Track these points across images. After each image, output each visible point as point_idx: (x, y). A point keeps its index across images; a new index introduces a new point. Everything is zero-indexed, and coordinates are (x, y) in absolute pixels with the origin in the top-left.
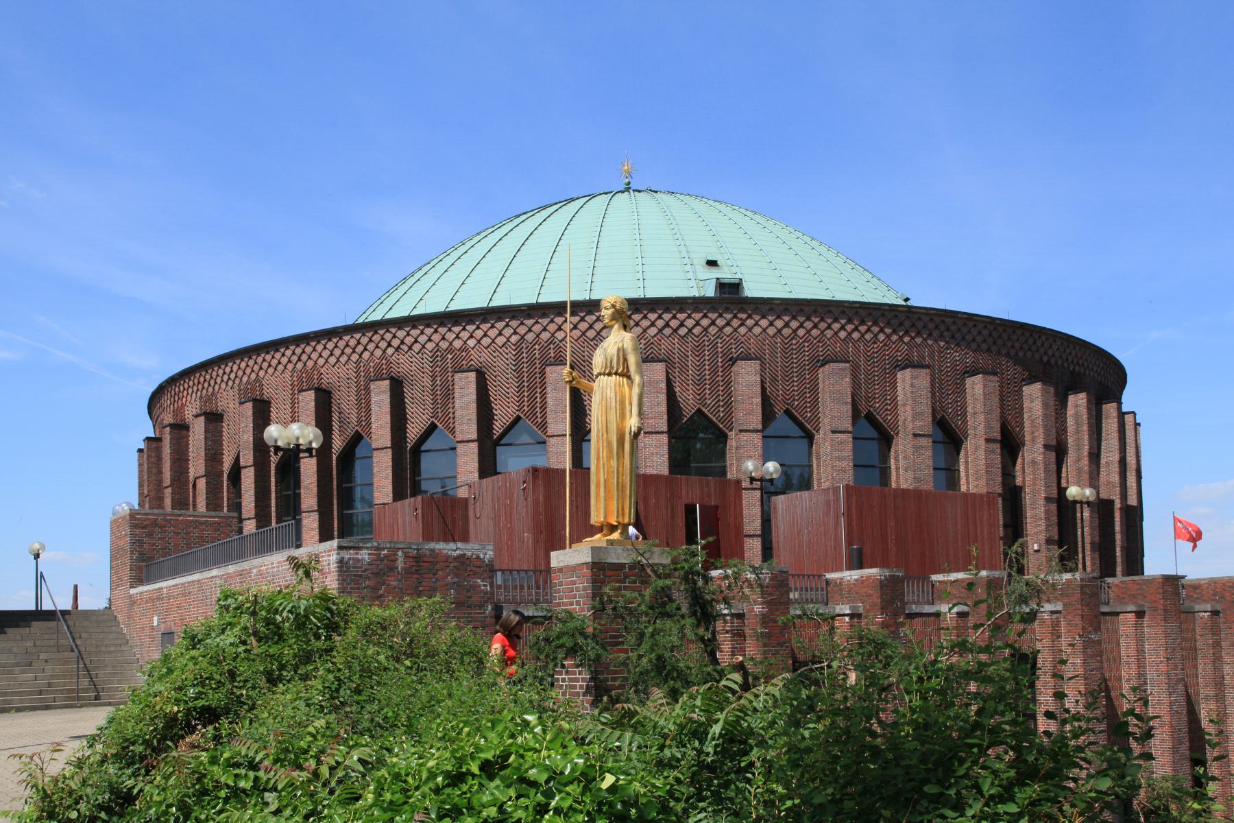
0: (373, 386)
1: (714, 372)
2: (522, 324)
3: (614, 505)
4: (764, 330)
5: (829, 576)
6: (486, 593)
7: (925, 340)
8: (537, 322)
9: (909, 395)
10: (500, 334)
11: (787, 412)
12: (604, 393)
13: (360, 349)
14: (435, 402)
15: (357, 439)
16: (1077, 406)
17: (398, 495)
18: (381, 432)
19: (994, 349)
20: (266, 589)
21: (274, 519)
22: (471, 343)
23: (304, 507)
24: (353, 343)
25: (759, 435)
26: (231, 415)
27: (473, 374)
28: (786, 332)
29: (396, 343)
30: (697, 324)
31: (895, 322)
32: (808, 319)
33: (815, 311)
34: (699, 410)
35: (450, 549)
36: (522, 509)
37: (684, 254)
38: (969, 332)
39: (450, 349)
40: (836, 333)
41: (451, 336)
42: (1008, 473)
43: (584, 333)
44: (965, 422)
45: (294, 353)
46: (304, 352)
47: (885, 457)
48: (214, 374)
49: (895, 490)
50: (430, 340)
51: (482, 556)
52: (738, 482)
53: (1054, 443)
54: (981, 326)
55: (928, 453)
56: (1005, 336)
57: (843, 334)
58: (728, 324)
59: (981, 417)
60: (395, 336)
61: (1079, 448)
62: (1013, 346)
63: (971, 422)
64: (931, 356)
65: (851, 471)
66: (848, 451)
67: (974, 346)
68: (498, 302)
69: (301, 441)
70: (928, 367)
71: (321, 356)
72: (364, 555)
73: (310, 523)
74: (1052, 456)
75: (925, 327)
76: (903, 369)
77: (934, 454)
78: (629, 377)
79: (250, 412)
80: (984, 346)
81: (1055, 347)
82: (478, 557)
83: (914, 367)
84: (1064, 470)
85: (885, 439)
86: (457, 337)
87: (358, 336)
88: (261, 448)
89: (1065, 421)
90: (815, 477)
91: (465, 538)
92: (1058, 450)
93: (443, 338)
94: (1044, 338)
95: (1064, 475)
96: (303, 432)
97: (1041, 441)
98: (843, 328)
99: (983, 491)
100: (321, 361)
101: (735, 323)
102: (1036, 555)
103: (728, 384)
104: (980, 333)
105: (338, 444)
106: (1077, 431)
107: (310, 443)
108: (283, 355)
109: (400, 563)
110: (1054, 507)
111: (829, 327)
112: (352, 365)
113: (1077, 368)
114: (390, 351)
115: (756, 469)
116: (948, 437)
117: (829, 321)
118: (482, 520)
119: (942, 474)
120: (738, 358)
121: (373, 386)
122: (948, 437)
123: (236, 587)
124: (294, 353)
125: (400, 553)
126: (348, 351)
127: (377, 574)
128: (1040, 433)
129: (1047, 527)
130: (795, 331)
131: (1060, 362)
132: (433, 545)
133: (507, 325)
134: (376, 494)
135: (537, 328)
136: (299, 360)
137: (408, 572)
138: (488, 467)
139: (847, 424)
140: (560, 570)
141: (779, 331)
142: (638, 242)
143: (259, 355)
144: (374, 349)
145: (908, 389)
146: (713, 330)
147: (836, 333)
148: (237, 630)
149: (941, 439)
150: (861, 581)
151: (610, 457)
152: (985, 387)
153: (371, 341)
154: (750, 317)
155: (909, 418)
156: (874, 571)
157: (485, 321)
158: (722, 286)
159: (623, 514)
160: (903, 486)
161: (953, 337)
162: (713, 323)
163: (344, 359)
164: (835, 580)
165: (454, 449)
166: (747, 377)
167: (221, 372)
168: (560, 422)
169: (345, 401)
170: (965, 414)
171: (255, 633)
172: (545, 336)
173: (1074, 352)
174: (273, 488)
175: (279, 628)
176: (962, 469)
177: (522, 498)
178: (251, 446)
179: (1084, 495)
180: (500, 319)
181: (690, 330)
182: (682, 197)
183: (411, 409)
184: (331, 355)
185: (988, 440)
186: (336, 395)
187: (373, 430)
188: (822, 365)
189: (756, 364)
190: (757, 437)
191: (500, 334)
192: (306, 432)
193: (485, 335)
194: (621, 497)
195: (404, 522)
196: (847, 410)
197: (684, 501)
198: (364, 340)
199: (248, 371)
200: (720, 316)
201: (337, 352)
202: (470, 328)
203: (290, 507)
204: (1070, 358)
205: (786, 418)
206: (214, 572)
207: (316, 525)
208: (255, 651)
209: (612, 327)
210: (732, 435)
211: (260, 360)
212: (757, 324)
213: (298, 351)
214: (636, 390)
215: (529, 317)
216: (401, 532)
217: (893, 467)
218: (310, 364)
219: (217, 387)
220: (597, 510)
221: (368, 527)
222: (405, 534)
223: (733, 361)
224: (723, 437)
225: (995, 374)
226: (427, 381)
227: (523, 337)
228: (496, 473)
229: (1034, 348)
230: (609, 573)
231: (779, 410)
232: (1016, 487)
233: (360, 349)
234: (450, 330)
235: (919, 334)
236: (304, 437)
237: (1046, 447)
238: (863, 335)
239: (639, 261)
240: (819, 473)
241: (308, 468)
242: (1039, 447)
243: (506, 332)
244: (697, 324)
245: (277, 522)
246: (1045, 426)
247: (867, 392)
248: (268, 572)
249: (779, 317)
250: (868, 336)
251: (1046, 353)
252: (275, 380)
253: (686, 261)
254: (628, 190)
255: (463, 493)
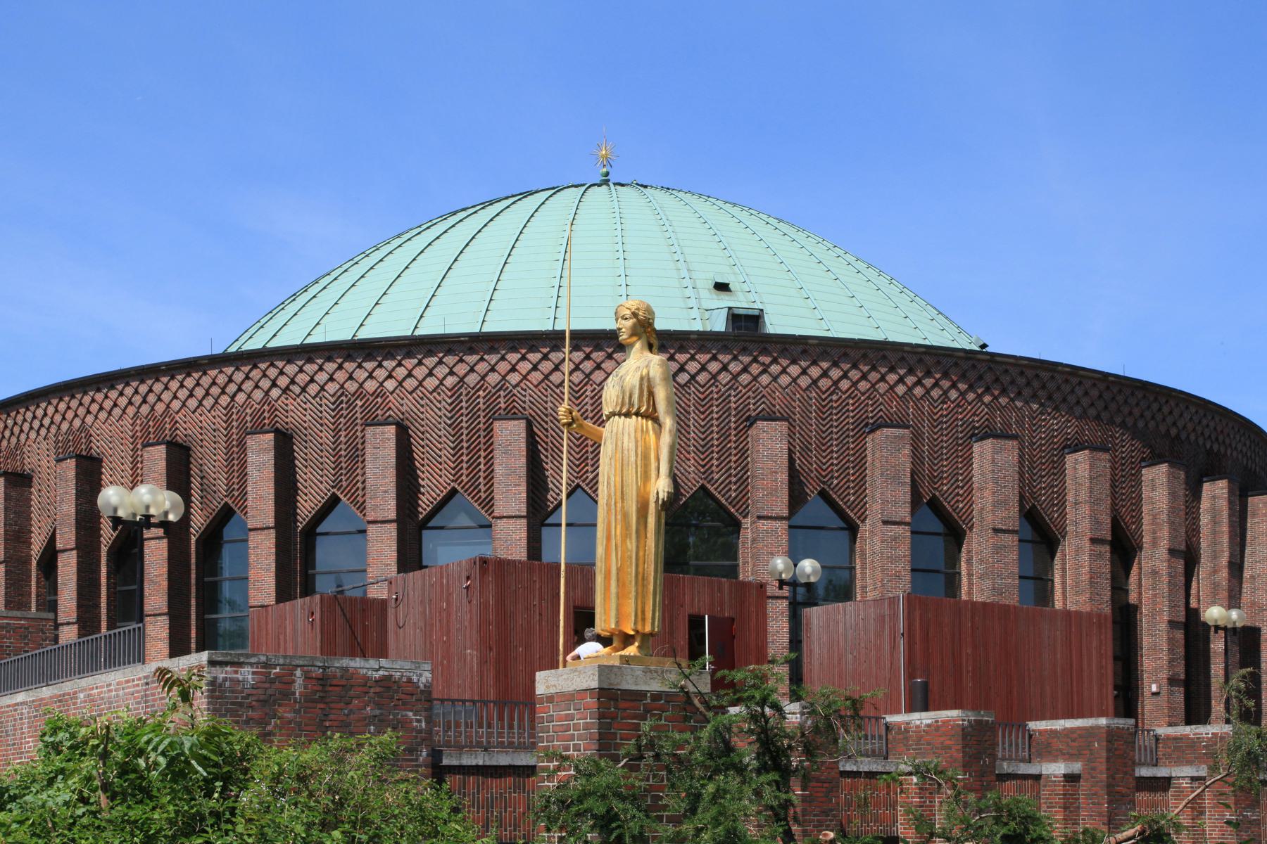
0: (251, 442)
1: (725, 436)
2: (461, 360)
3: (630, 607)
4: (794, 380)
5: (890, 719)
6: (420, 731)
7: (1012, 400)
8: (482, 359)
9: (989, 476)
10: (430, 374)
11: (823, 494)
12: (620, 439)
13: (232, 388)
14: (337, 465)
15: (225, 515)
16: (1214, 497)
17: (284, 593)
18: (260, 504)
19: (1104, 415)
20: (124, 716)
21: (104, 624)
22: (390, 385)
23: (148, 608)
24: (222, 379)
25: (785, 524)
26: (44, 476)
27: (392, 429)
28: (824, 383)
29: (283, 381)
30: (703, 368)
31: (972, 375)
32: (855, 366)
33: (864, 356)
34: (703, 487)
35: (368, 667)
36: (465, 616)
37: (684, 273)
38: (1072, 391)
39: (360, 393)
40: (892, 388)
41: (361, 375)
42: (1119, 587)
43: (546, 377)
44: (1063, 515)
45: (136, 392)
46: (151, 391)
47: (953, 560)
48: (20, 418)
49: (966, 602)
50: (331, 379)
51: (415, 679)
52: (762, 586)
53: (1183, 547)
54: (1088, 384)
55: (1012, 556)
56: (1120, 398)
57: (901, 389)
58: (745, 370)
59: (1085, 509)
60: (282, 373)
61: (1215, 556)
62: (1130, 413)
63: (1070, 516)
64: (1020, 423)
65: (908, 577)
66: (904, 550)
67: (1078, 411)
68: (425, 329)
69: (152, 511)
70: (1014, 437)
71: (175, 397)
72: (247, 674)
73: (157, 631)
74: (1180, 565)
75: (1013, 382)
76: (982, 439)
77: (1020, 554)
78: (656, 420)
79: (72, 474)
80: (1092, 412)
81: (1187, 416)
82: (410, 680)
83: (996, 436)
84: (1194, 584)
85: (955, 534)
86: (371, 376)
87: (229, 370)
88: (88, 517)
89: (1198, 518)
90: (858, 583)
91: (382, 652)
92: (1188, 557)
93: (351, 378)
94: (1172, 403)
95: (1193, 591)
96: (152, 498)
97: (1165, 544)
98: (901, 380)
99: (1086, 608)
100: (176, 405)
101: (755, 369)
102: (1155, 698)
103: (743, 453)
104: (1086, 393)
105: (199, 521)
106: (1214, 532)
107: (166, 513)
108: (121, 394)
109: (298, 686)
110: (1180, 635)
111: (883, 379)
112: (219, 412)
113: (1216, 447)
114: (275, 393)
115: (786, 569)
116: (1040, 534)
117: (883, 370)
118: (406, 628)
119: (1030, 584)
120: (757, 418)
121: (251, 442)
122: (1040, 534)
123: (74, 715)
124: (136, 392)
125: (298, 672)
126: (215, 391)
127: (264, 702)
128: (1164, 533)
129: (1171, 661)
130: (836, 383)
131: (1192, 437)
132: (346, 662)
133: (440, 362)
134: (252, 592)
135: (482, 368)
136: (144, 401)
137: (309, 699)
138: (410, 558)
139: (904, 512)
140: (550, 699)
141: (815, 382)
142: (620, 255)
143: (85, 393)
144: (253, 390)
145: (988, 467)
146: (724, 378)
147: (892, 388)
148: (74, 781)
149: (1029, 538)
150: (935, 728)
151: (626, 536)
152: (1092, 467)
153: (247, 378)
154: (775, 361)
155: (989, 507)
156: (954, 713)
157: (409, 355)
158: (735, 318)
159: (644, 620)
160: (977, 598)
161: (1050, 398)
162: (725, 368)
163: (208, 402)
164: (899, 725)
165: (365, 531)
166: (769, 443)
167: (29, 415)
168: (511, 497)
169: (210, 463)
170: (1063, 503)
171: (106, 787)
172: (493, 378)
173: (1212, 424)
174: (104, 581)
175: (142, 778)
176: (1057, 579)
177: (464, 601)
178: (73, 522)
179: (1229, 618)
180: (430, 353)
181: (693, 377)
182: (681, 195)
183: (305, 476)
184: (191, 395)
185: (1093, 541)
186: (197, 452)
187: (249, 503)
188: (872, 431)
189: (782, 427)
190: (781, 526)
191: (430, 374)
192: (160, 498)
193: (410, 375)
194: (641, 595)
195: (295, 631)
196: (904, 494)
197: (688, 610)
198: (239, 377)
199: (70, 415)
200: (735, 358)
201: (199, 392)
202: (389, 364)
203: (129, 607)
204: (1207, 432)
205: (821, 502)
206: (21, 697)
207: (165, 634)
208: (106, 815)
209: (632, 345)
210: (747, 523)
211: (87, 400)
212: (784, 371)
213: (143, 389)
214: (666, 439)
215: (472, 351)
216: (289, 645)
217: (964, 573)
218: (160, 407)
219: (23, 437)
220: (606, 612)
221: (239, 638)
222: (296, 648)
223: (751, 421)
224: (736, 526)
225: (1106, 450)
226: (327, 437)
227: (462, 380)
228: (421, 567)
229: (1159, 417)
230: (622, 704)
231: (812, 492)
232: (1128, 605)
233: (232, 388)
234: (360, 366)
235: (1004, 392)
236: (156, 504)
237: (1172, 552)
238: (928, 392)
239: (622, 281)
240: (863, 578)
241: (156, 553)
242: (1163, 553)
243: (438, 373)
244: (703, 368)
245: (108, 629)
246: (1171, 523)
247: (931, 470)
248: (115, 694)
249: (814, 363)
250: (936, 393)
251: (1174, 424)
252: (110, 429)
253: (687, 282)
254: (606, 182)
255: (378, 592)
